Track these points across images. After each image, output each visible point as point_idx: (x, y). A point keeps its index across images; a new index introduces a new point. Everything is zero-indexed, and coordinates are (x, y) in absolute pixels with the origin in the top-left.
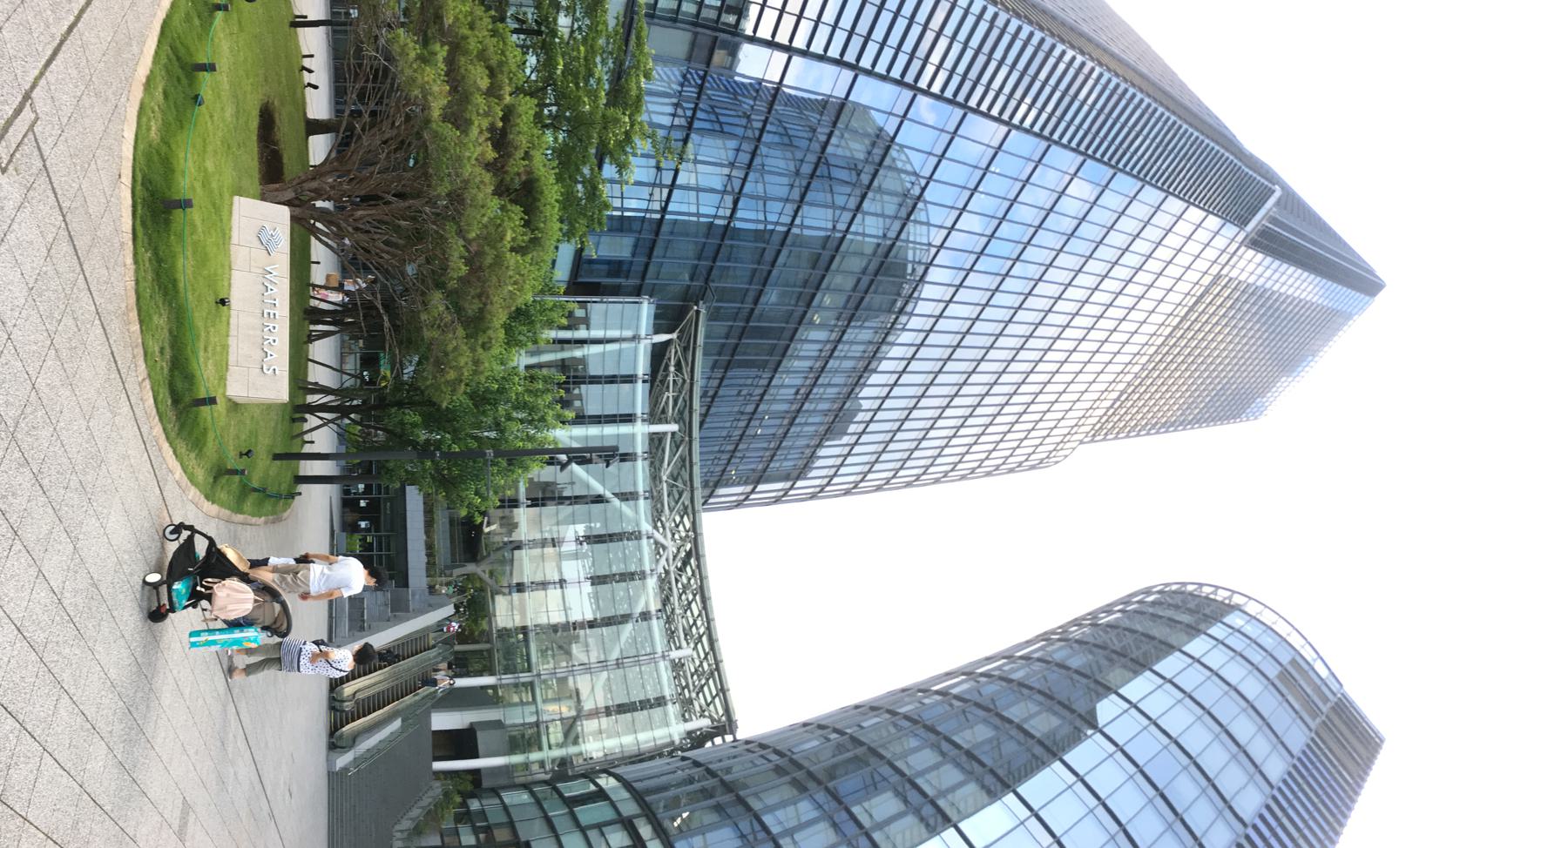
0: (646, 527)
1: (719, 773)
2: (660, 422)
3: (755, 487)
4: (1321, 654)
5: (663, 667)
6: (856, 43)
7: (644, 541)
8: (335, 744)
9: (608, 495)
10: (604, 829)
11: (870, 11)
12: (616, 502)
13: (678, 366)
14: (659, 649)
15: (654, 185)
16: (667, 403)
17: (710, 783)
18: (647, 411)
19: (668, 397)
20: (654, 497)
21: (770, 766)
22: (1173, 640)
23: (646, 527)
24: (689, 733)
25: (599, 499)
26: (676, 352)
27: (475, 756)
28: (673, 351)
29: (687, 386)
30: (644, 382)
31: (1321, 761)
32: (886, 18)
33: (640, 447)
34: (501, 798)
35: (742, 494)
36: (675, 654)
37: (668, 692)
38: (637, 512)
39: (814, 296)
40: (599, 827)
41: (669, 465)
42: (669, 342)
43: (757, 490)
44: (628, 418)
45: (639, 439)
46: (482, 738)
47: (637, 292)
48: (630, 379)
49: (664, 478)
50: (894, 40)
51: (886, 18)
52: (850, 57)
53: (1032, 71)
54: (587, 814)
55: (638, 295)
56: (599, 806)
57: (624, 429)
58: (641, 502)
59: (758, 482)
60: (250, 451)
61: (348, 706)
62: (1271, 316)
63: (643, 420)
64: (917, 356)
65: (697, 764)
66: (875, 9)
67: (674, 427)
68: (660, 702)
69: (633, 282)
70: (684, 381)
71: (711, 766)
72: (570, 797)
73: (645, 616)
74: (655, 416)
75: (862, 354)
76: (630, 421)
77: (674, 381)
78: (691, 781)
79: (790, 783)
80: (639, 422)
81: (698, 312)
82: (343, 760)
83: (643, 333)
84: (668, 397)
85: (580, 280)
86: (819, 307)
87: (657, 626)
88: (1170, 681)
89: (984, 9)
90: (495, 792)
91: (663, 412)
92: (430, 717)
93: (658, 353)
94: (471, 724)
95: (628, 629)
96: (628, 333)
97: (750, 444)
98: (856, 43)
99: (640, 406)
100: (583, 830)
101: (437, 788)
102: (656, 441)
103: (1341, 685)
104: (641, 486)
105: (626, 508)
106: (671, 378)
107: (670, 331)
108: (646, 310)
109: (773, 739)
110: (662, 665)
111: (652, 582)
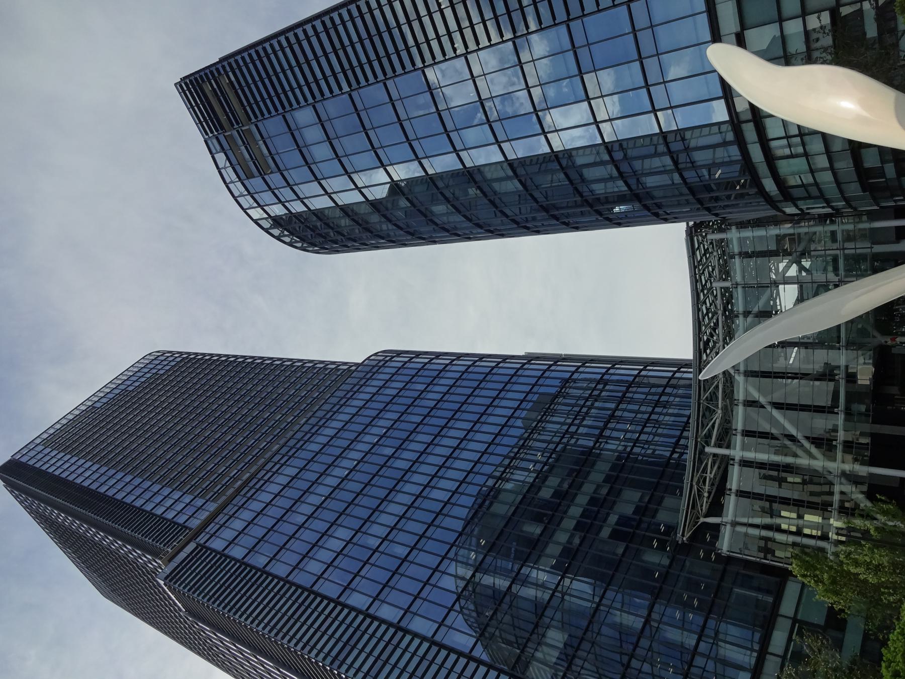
2: (724, 456)
4: (217, 171)
6: (430, 656)
9: (769, 408)
11: (419, 673)
12: (762, 400)
13: (700, 495)
15: (461, 547)
17: (705, 196)
18: (730, 467)
19: (711, 473)
22: (338, 213)
25: (778, 406)
26: (702, 506)
28: (704, 508)
29: (695, 479)
30: (730, 490)
31: (170, 534)
32: (410, 669)
33: (738, 439)
36: (727, 284)
37: (737, 261)
38: (746, 390)
39: (513, 514)
41: (714, 423)
42: (706, 516)
44: (745, 463)
47: (729, 560)
48: (741, 494)
49: (719, 411)
50: (407, 656)
51: (410, 669)
52: (434, 649)
53: (316, 614)
55: (729, 558)
57: (750, 455)
62: (125, 448)
64: (364, 454)
65: (709, 210)
66: (416, 674)
68: (745, 255)
73: (746, 314)
74: (725, 463)
75: (515, 472)
76: (744, 461)
78: (717, 199)
80: (737, 459)
81: (683, 535)
83: (728, 527)
84: (711, 473)
85: (778, 579)
86: (511, 506)
87: (740, 307)
88: (346, 172)
89: (355, 675)
91: (714, 463)
93: (716, 508)
96: (740, 529)
97: (560, 429)
98: (430, 656)
99: (735, 472)
102: (724, 439)
103: (206, 142)
104: (740, 411)
105: (756, 395)
106: (707, 488)
107: (704, 523)
108: (725, 545)
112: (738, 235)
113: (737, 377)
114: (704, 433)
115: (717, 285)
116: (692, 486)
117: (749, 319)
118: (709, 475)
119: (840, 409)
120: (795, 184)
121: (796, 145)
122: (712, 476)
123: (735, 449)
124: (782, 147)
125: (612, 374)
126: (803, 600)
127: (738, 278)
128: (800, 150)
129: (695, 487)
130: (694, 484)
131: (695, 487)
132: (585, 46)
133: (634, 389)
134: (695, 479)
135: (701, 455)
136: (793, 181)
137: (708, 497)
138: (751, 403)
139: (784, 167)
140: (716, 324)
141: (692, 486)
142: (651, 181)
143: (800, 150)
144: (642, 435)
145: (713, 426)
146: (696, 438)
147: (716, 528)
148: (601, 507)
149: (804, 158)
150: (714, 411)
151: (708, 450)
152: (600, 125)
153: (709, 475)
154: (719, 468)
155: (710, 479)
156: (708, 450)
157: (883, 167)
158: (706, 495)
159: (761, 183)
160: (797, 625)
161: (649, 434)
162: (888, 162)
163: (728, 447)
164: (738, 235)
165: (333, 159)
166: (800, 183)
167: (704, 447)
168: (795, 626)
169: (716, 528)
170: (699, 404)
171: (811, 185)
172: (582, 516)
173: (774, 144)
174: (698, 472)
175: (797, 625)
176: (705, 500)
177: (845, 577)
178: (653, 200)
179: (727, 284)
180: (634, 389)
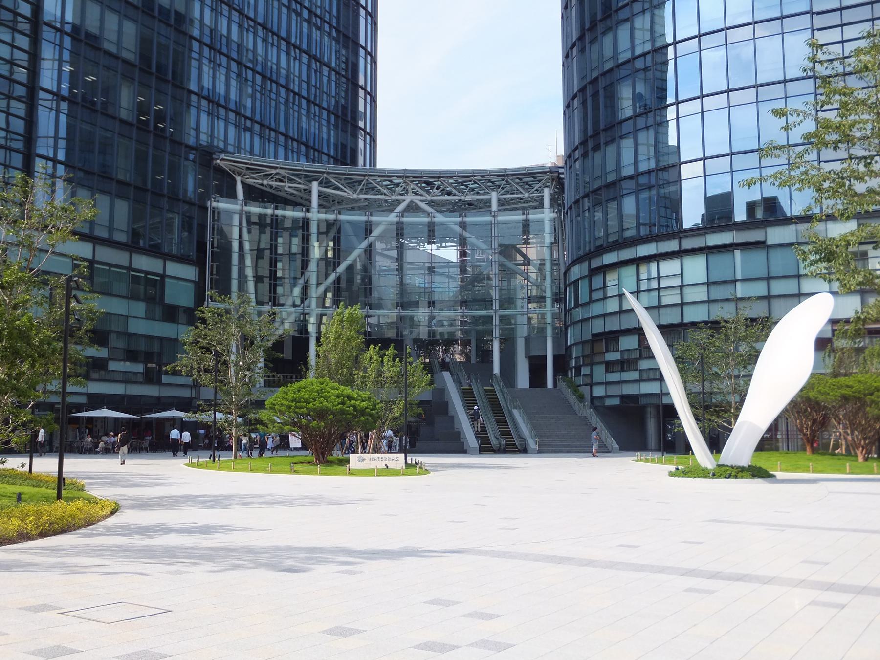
0: (392, 217)
1: (578, 197)
3: (362, 47)
5: (503, 218)
7: (405, 220)
8: (524, 450)
10: (593, 289)
14: (488, 219)
16: (295, 188)
19: (290, 187)
20: (368, 207)
21: (581, 159)
23: (392, 217)
24: (552, 206)
27: (545, 357)
29: (282, 172)
30: (276, 208)
34: (571, 346)
35: (366, 59)
36: (494, 206)
38: (379, 224)
40: (591, 291)
41: (342, 190)
42: (242, 183)
43: (364, 45)
45: (323, 216)
46: (535, 353)
49: (355, 196)
54: (583, 297)
56: (581, 285)
58: (374, 219)
59: (357, 44)
60: (749, 187)
61: (503, 442)
63: (308, 211)
67: (315, 187)
69: (195, 212)
70: (277, 174)
71: (573, 201)
72: (575, 304)
77: (276, 181)
79: (594, 152)
80: (309, 215)
81: (223, 160)
82: (532, 444)
90: (568, 348)
92: (388, 175)
94: (526, 357)
95: (472, 239)
100: (591, 301)
101: (562, 385)
106: (274, 184)
107: (235, 181)
109: (567, 151)
110: (500, 218)
111: (439, 218)
112: (547, 219)
113: (393, 214)
114: (333, 181)
115: (494, 196)
116: (276, 168)
117: (457, 229)
118: (286, 186)
119: (369, 311)
120: (608, 279)
121: (649, 285)
122: (286, 189)
123: (319, 212)
124: (649, 272)
125: (366, 59)
126: (181, 282)
127: (500, 218)
128: (644, 286)
129: (274, 171)
130: (278, 171)
131: (274, 171)
132: (785, 85)
133: (333, 78)
134: (282, 172)
135: (310, 178)
136: (612, 278)
137: (262, 185)
138: (368, 229)
139: (629, 273)
140: (449, 194)
141: (276, 168)
142: (627, 145)
143: (644, 286)
144: (223, 51)
145: (337, 188)
146: (328, 173)
147: (232, 195)
148: (176, 29)
149: (636, 290)
150: (355, 191)
151: (315, 185)
152: (699, 100)
153: (286, 186)
154: (292, 194)
155: (282, 187)
156: (315, 185)
157: (618, 351)
158: (265, 182)
159: (616, 250)
160: (159, 278)
161: (253, 82)
162: (622, 355)
163: (320, 206)
164: (547, 219)
165: (842, 22)
166: (608, 284)
167: (316, 180)
168: (158, 276)
169: (232, 195)
170: (364, 176)
171: (605, 293)
172: (176, 13)
173: (653, 266)
174: (288, 173)
175: (159, 278)
176: (260, 182)
177: (324, 351)
178: (604, 144)
179: (494, 206)
180: (333, 78)
